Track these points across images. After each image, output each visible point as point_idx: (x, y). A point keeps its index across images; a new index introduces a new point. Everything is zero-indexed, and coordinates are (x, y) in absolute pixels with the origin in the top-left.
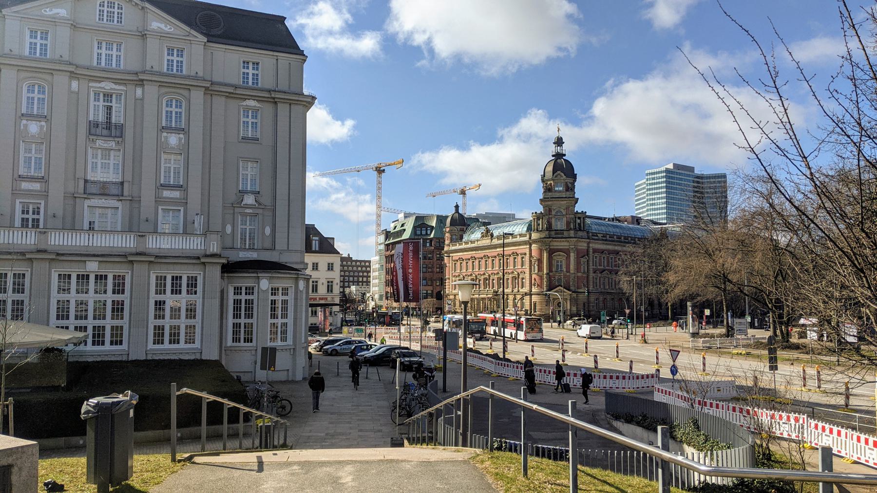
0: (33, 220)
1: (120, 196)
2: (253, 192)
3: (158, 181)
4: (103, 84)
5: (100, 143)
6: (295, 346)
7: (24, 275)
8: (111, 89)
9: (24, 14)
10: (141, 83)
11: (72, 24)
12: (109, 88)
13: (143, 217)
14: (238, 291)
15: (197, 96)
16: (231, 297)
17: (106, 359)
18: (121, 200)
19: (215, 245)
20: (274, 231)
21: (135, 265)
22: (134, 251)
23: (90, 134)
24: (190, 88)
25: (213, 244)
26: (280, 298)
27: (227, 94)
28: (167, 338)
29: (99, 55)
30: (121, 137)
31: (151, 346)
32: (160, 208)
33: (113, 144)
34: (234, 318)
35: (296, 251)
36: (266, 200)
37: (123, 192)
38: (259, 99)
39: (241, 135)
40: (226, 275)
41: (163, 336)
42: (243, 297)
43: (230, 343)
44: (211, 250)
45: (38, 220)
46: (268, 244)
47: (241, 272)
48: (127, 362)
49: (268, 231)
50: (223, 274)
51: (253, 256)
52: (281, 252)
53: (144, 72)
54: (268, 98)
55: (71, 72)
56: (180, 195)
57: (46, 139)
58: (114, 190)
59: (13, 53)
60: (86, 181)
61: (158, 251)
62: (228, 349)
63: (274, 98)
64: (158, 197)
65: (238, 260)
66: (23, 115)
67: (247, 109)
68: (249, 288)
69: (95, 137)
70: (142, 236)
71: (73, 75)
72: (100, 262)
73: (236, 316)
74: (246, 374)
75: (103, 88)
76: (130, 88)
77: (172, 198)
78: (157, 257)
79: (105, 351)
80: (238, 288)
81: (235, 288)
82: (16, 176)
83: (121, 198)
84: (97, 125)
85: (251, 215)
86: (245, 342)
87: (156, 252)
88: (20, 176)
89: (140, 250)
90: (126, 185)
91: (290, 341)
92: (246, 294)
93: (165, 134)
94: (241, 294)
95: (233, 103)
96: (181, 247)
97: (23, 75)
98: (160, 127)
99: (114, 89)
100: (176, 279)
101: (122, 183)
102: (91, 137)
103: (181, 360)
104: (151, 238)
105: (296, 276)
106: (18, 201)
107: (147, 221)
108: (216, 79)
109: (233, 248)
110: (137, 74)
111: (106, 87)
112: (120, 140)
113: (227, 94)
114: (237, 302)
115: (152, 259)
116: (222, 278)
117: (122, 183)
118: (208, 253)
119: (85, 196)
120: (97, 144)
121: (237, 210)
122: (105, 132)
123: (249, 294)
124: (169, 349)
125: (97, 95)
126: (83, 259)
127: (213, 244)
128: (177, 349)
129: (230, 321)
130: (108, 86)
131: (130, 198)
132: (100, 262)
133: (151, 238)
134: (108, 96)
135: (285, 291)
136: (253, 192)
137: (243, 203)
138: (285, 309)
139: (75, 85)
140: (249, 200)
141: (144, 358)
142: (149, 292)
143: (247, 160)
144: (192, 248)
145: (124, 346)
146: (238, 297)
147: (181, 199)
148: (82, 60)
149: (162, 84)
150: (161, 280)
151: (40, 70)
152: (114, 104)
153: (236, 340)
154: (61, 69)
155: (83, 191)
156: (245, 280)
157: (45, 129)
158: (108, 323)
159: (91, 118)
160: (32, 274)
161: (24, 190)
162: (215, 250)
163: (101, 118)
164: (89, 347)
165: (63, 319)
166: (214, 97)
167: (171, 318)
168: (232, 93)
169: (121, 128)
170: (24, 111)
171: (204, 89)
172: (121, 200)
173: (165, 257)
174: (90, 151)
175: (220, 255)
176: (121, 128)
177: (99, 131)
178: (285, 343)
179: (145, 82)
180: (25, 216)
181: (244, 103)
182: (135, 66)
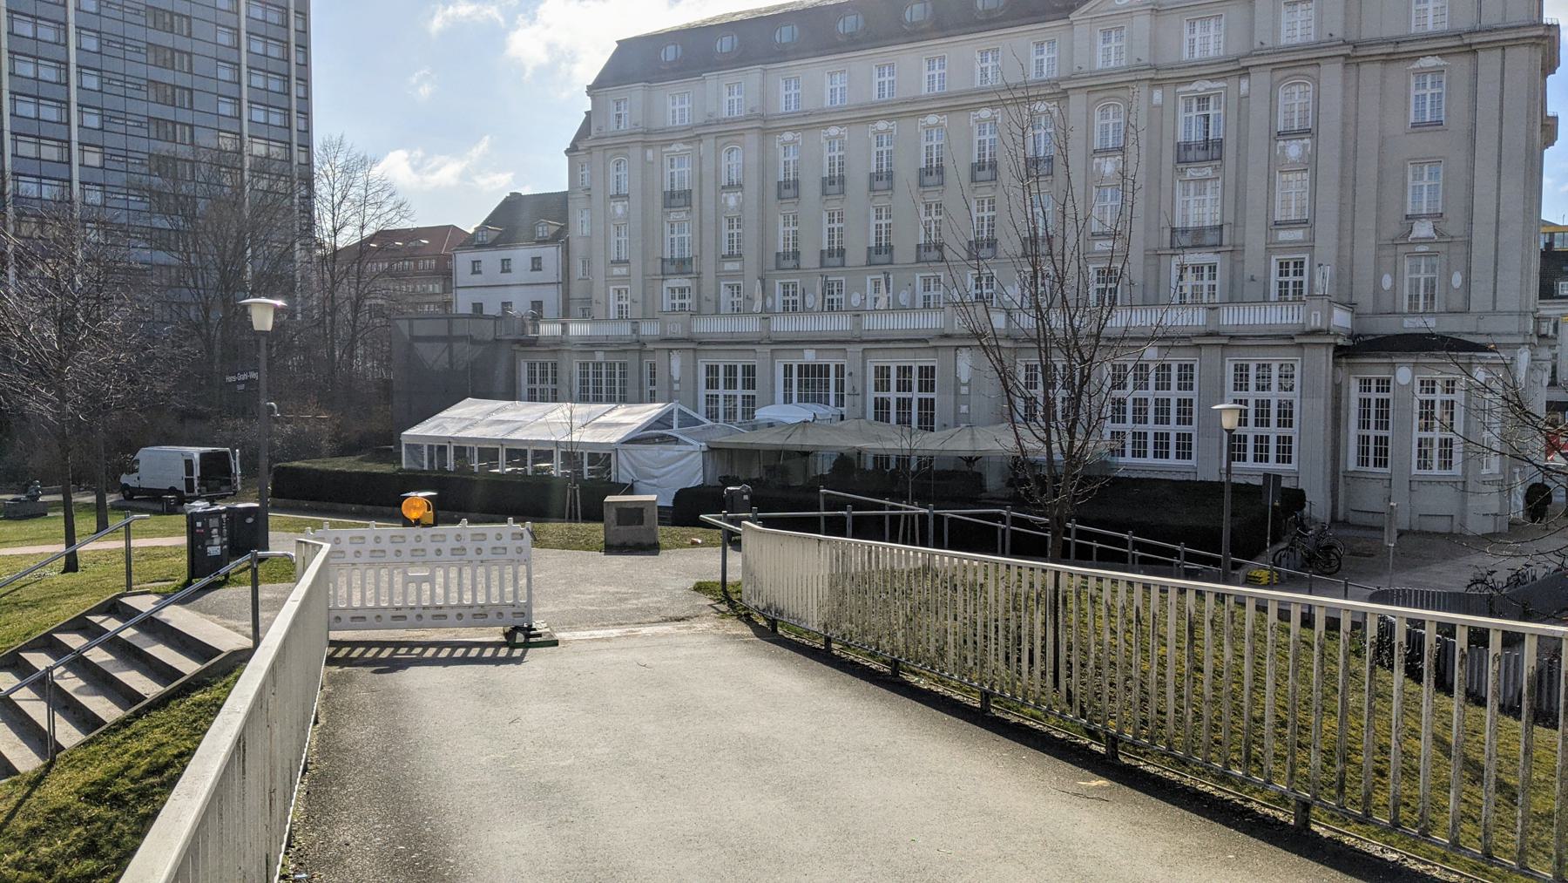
0: (1295, 283)
1: (1217, 247)
2: (1429, 216)
3: (1270, 217)
4: (1194, 86)
5: (1191, 173)
6: (1466, 477)
7: (1192, 366)
8: (1207, 90)
9: (1095, 13)
10: (1245, 72)
11: (1152, 10)
12: (1203, 89)
13: (1247, 276)
14: (1365, 385)
15: (1332, 73)
16: (1354, 394)
17: (1153, 476)
18: (1219, 252)
19: (1319, 316)
20: (1467, 281)
21: (1306, 351)
22: (1202, 330)
23: (1178, 162)
24: (1318, 61)
25: (1316, 315)
26: (1439, 396)
27: (1384, 57)
28: (1273, 453)
29: (674, 112)
30: (1220, 158)
31: (1415, 471)
32: (722, 283)
33: (1209, 170)
34: (1359, 428)
35: (1510, 313)
36: (1454, 227)
37: (1221, 240)
38: (1442, 53)
39: (1412, 119)
40: (1344, 360)
41: (1167, 447)
42: (1374, 395)
43: (1352, 465)
44: (1313, 324)
45: (1301, 283)
46: (1457, 302)
47: (1369, 356)
48: (1195, 482)
49: (1457, 280)
50: (1336, 360)
51: (1431, 324)
52: (1481, 315)
53: (1249, 55)
54: (1459, 46)
55: (1151, 79)
56: (1304, 235)
57: (1310, 164)
58: (1210, 238)
59: (1265, 47)
60: (1173, 230)
61: (1235, 329)
62: (1352, 476)
63: (1470, 45)
64: (1271, 243)
65: (1401, 331)
66: (1095, 151)
67: (1422, 73)
68: (1383, 381)
69: (1184, 166)
70: (858, 315)
71: (1155, 83)
72: (816, 349)
73: (1364, 424)
74: (1376, 515)
75: (1196, 91)
76: (1233, 81)
77: (1290, 242)
78: (1232, 337)
79: (1171, 466)
80: (1383, 381)
81: (1361, 381)
82: (1271, 223)
83: (1219, 249)
84: (1187, 146)
85: (1428, 255)
86: (1375, 466)
87: (1233, 331)
88: (1093, 234)
89: (1211, 328)
90: (1226, 230)
91: (1457, 469)
92: (1378, 391)
93: (1281, 143)
94: (1369, 391)
95: (1396, 71)
96: (1236, 323)
97: (1280, 75)
98: (1274, 134)
99: (1210, 89)
100: (731, 370)
101: (1221, 227)
102: (1179, 166)
103: (1247, 485)
104: (1226, 311)
105: (1468, 361)
106: (1273, 259)
107: (1253, 280)
108: (1366, 35)
109: (1395, 313)
110: (1237, 60)
111: (1199, 89)
112: (1218, 163)
113: (1384, 57)
114: (1365, 403)
115: (1225, 341)
116: (1335, 364)
117: (1221, 227)
118: (1307, 329)
119: (1172, 252)
120: (1188, 175)
121: (1401, 249)
122: (1201, 155)
123: (1383, 391)
124: (1154, 466)
125: (1188, 100)
126: (800, 347)
127: (1316, 315)
128: (1164, 466)
129: (1353, 431)
130: (1201, 87)
131: (1230, 248)
132: (816, 349)
133: (1226, 311)
134: (1203, 100)
135: (1450, 386)
136: (1429, 216)
137: (1411, 236)
138: (1364, 414)
139: (1157, 95)
140: (1423, 230)
141: (1217, 480)
142: (1222, 387)
143: (1419, 162)
144: (1273, 322)
145: (1293, 466)
146: (1366, 395)
147: (1305, 241)
148: (1168, 58)
149: (1091, 90)
150: (712, 370)
151: (1304, 63)
152: (1211, 112)
153: (1363, 461)
154: (1262, 62)
155: (774, 267)
156: (1375, 369)
157: (1309, 149)
158: (1173, 428)
159: (1181, 138)
160: (1302, 366)
161: (1281, 243)
162: (1319, 324)
163: (1196, 136)
164: (1128, 459)
165: (1184, 424)
166: (1507, 50)
167: (1156, 423)
168: (1394, 53)
169: (1220, 144)
170: (1097, 146)
171: (1342, 59)
172: (1219, 252)
173: (1244, 337)
174: (1178, 185)
175: (1328, 331)
176: (1220, 144)
177: (1191, 155)
178: (1447, 472)
179: (1069, 92)
180: (1284, 279)
181: (1416, 65)
182: (1237, 49)
